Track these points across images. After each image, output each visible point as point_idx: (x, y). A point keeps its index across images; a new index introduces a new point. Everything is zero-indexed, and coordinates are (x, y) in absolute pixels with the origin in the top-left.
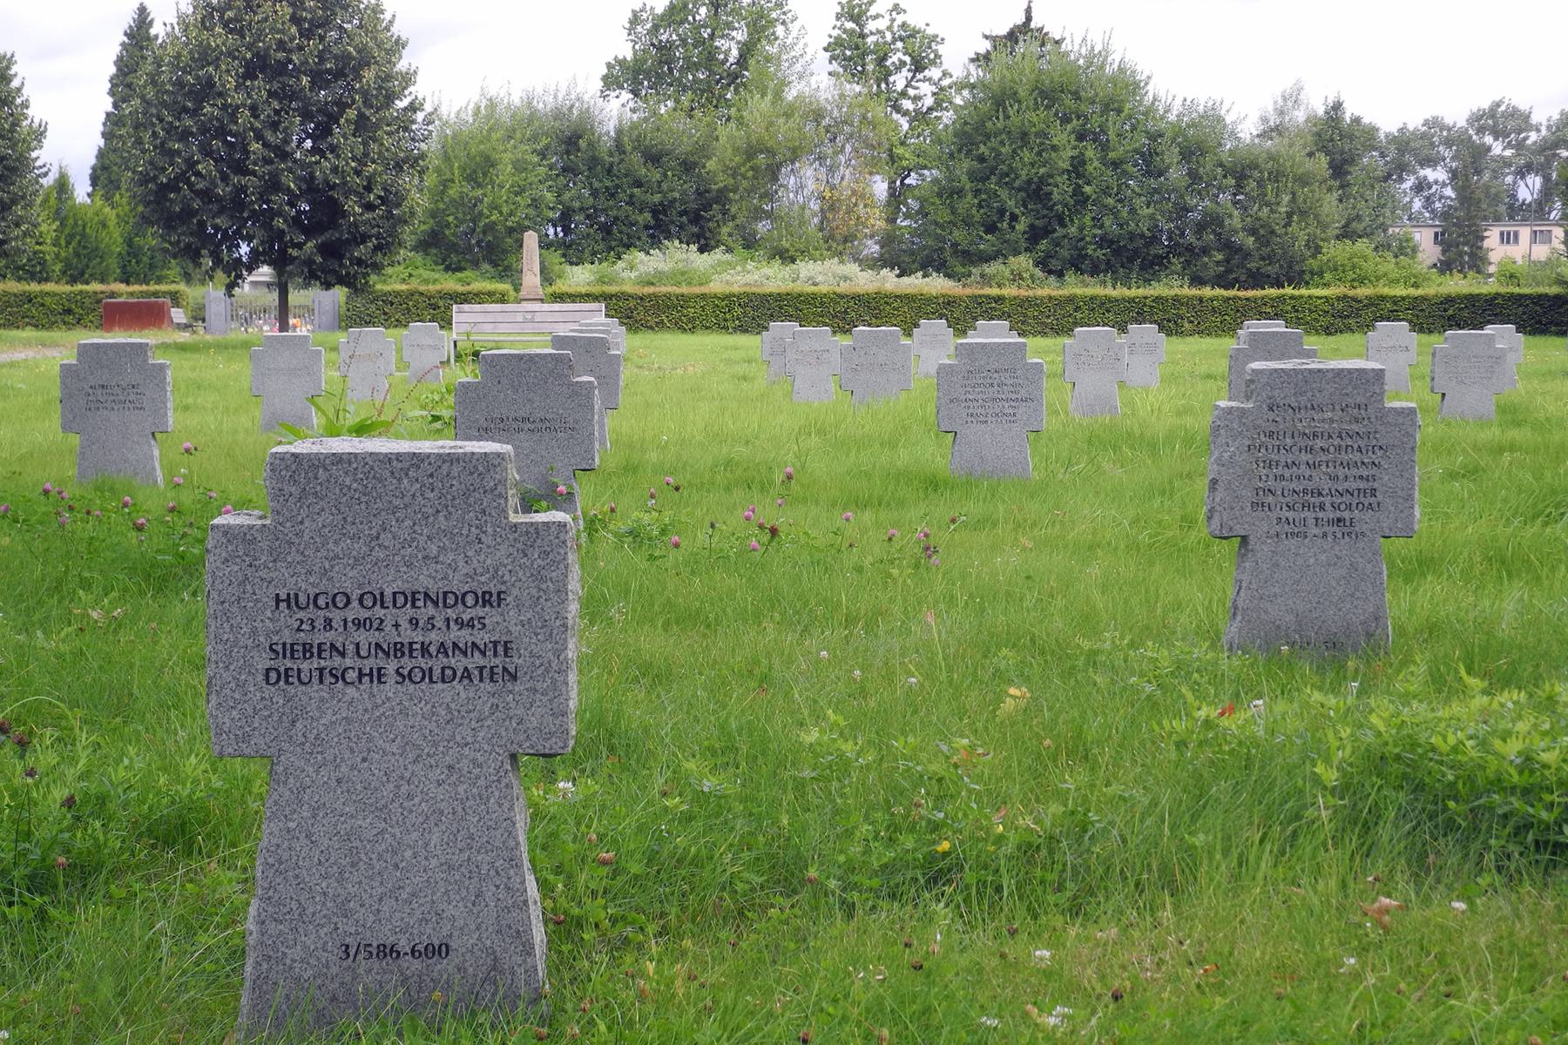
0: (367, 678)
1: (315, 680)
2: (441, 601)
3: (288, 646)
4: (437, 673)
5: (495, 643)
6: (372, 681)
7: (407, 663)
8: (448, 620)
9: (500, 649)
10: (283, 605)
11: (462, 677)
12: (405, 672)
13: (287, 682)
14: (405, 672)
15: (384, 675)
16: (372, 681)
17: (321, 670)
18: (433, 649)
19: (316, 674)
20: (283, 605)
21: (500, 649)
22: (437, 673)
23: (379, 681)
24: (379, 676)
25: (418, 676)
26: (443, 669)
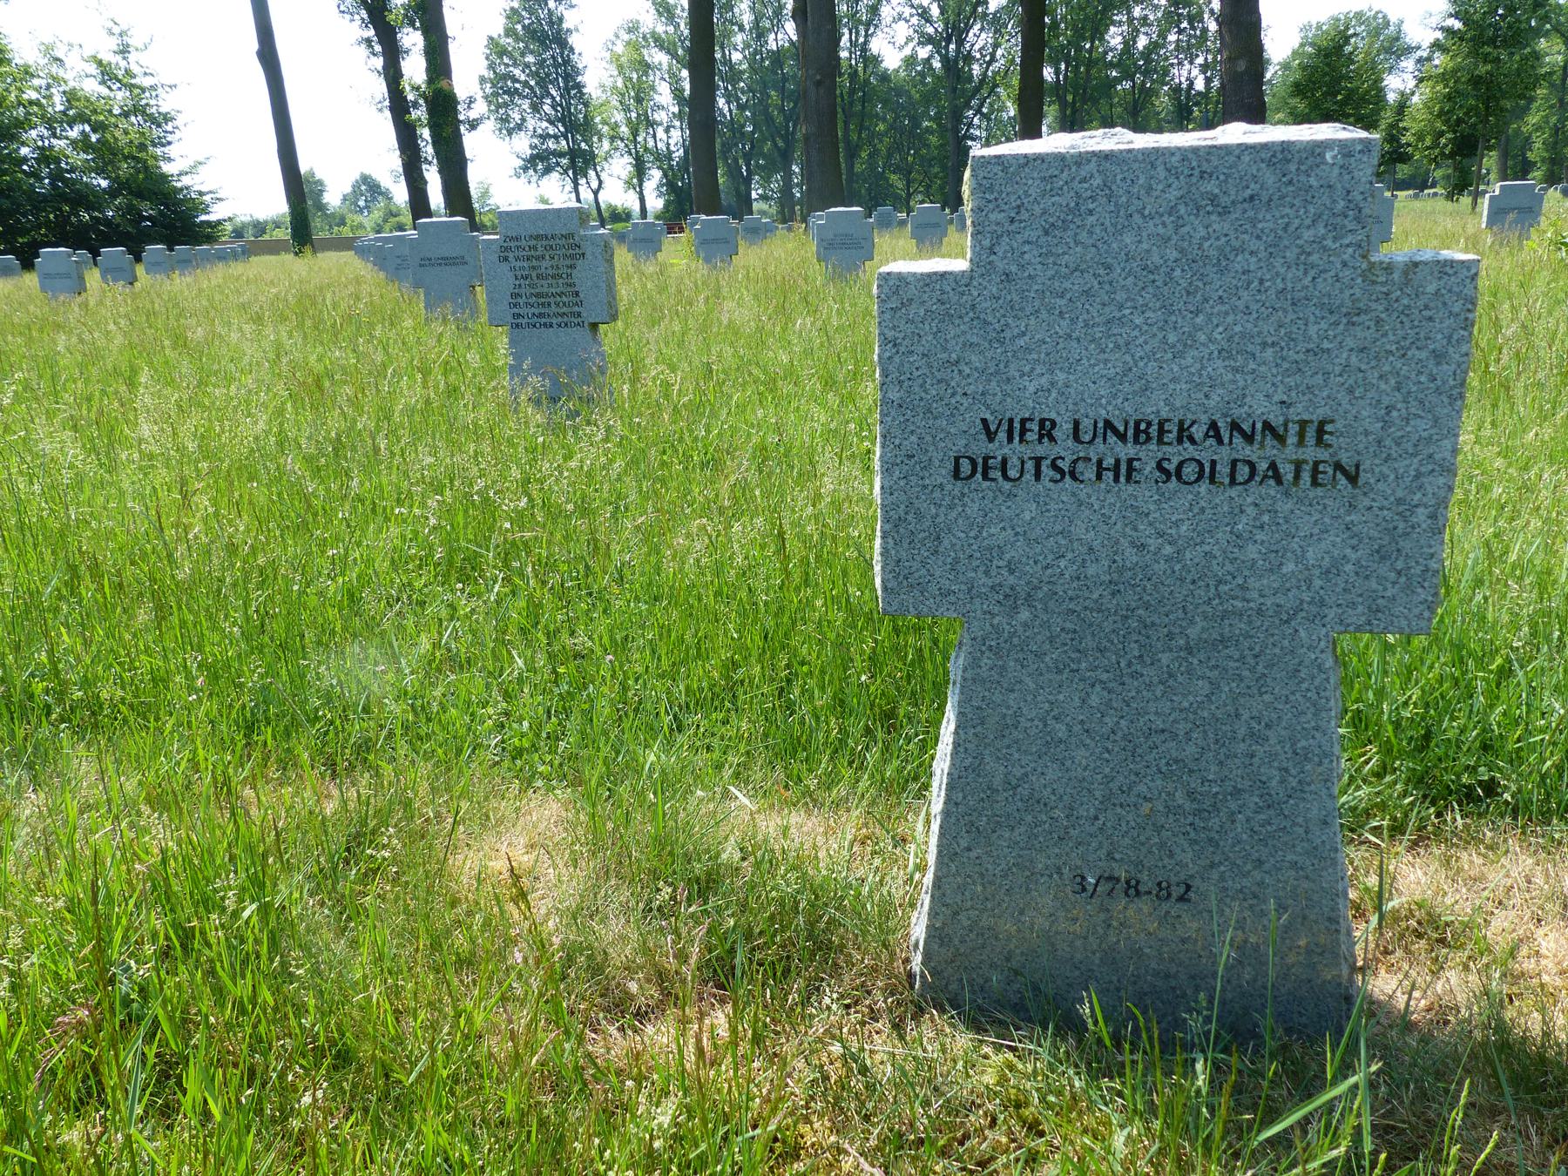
0: (1110, 475)
1: (1029, 476)
2: (1100, 431)
3: (1017, 425)
4: (1223, 470)
5: (1303, 424)
6: (1116, 479)
7: (1175, 454)
8: (1038, 461)
9: (1311, 433)
10: (1109, 476)
11: (1265, 477)
12: (1171, 467)
13: (985, 477)
14: (1171, 467)
15: (1139, 471)
16: (1116, 479)
17: (1038, 461)
18: (1198, 432)
19: (1030, 465)
20: (1109, 476)
21: (1311, 433)
22: (1223, 470)
23: (1129, 478)
24: (1127, 471)
25: (1190, 471)
26: (1234, 463)
